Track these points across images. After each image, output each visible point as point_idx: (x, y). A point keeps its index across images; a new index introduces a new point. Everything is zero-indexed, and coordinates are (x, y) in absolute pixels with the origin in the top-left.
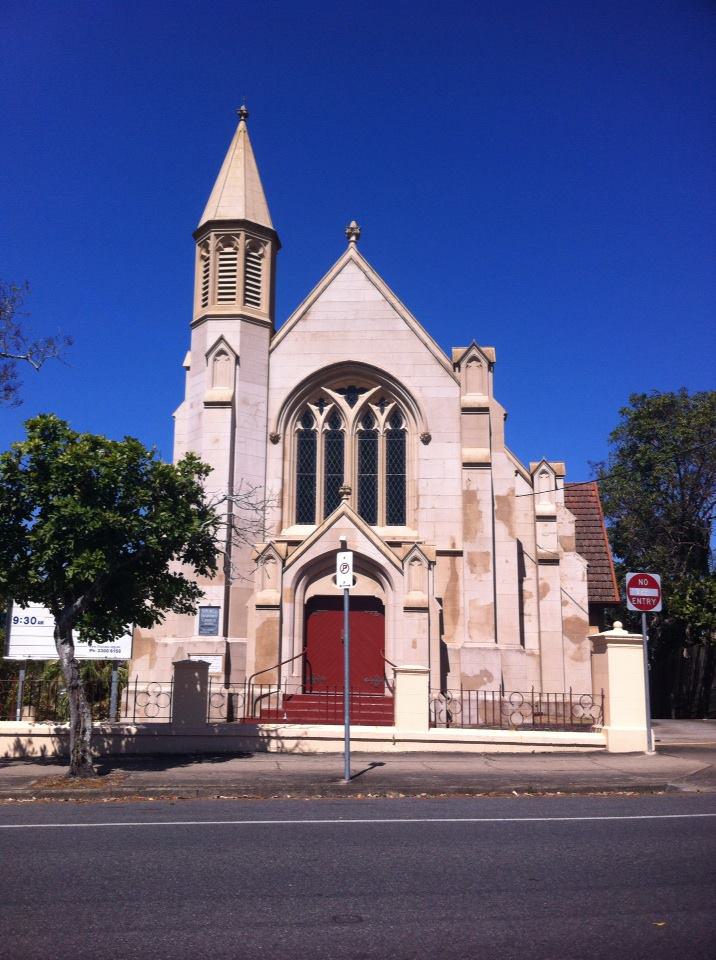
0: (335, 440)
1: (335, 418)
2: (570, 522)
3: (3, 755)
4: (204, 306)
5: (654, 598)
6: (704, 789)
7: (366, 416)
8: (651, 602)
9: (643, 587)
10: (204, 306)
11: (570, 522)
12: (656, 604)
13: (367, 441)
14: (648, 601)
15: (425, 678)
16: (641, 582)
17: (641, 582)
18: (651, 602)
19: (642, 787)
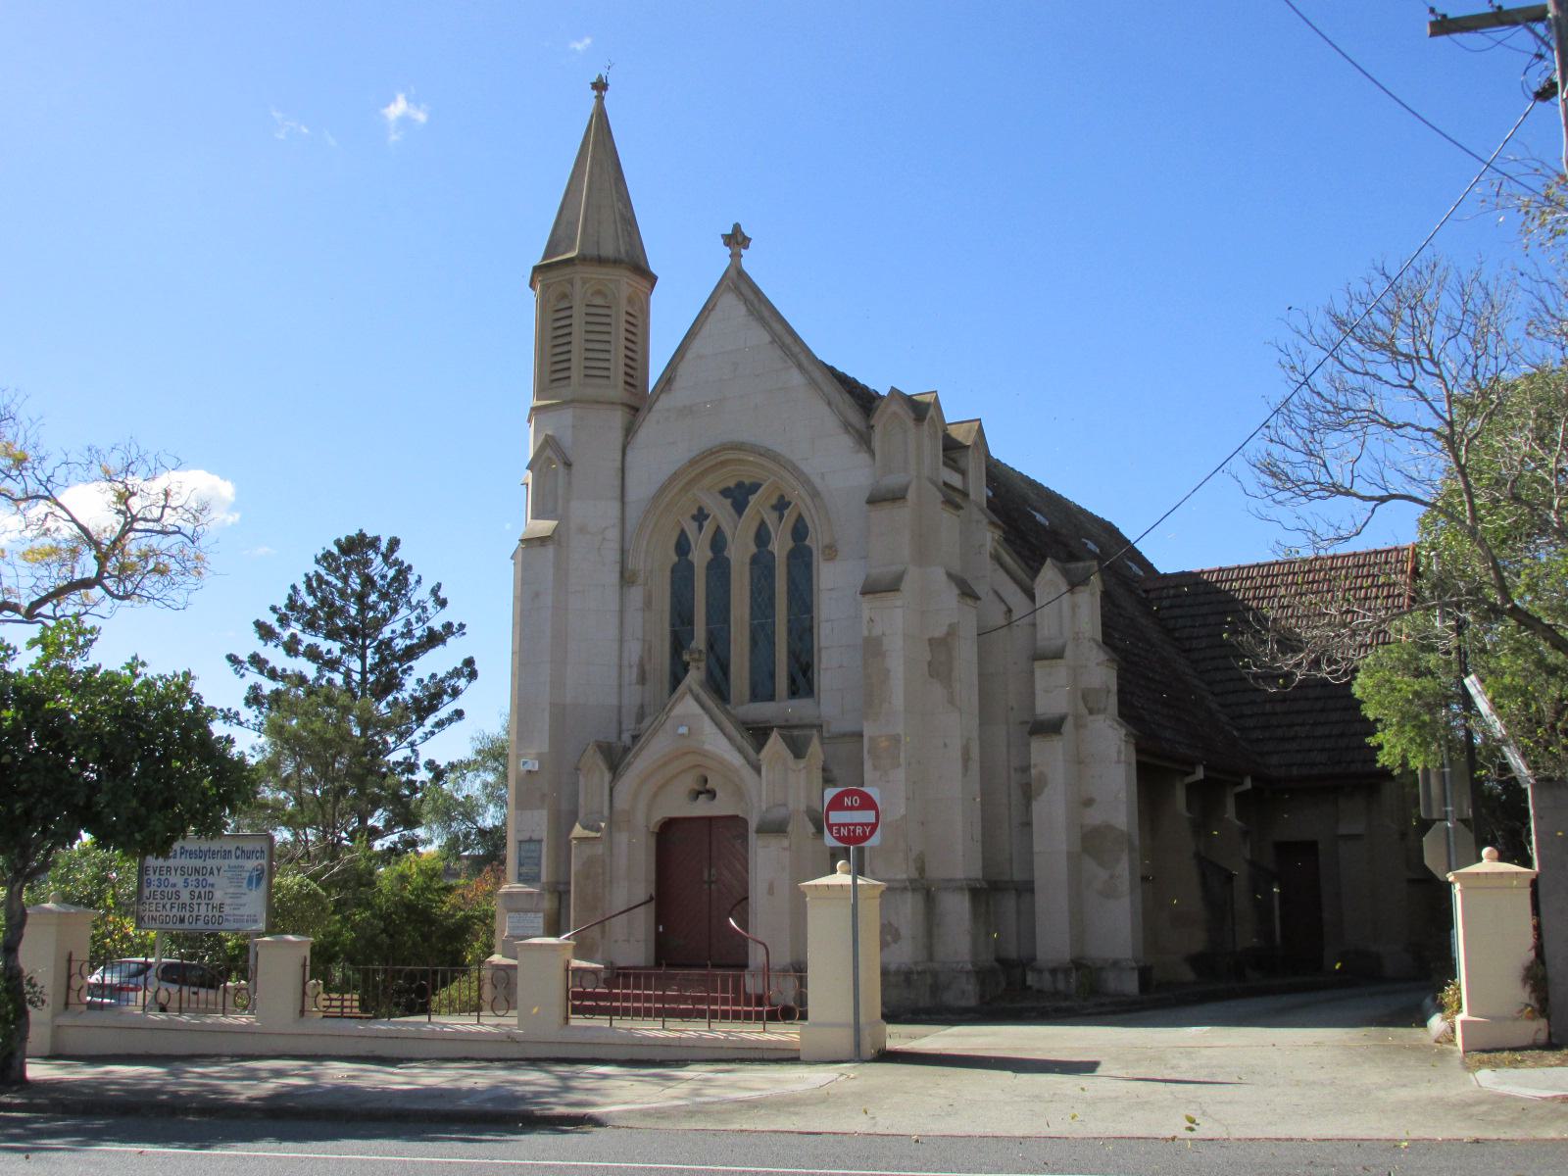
0: (719, 567)
1: (718, 543)
2: (1098, 664)
3: (1062, 730)
4: (233, 659)
5: (867, 825)
6: (787, 1075)
7: (762, 537)
8: (864, 832)
9: (851, 808)
10: (233, 659)
11: (1098, 664)
12: (872, 832)
13: (762, 564)
14: (859, 830)
15: (831, 822)
16: (847, 801)
17: (847, 801)
18: (864, 832)
19: (677, 1017)
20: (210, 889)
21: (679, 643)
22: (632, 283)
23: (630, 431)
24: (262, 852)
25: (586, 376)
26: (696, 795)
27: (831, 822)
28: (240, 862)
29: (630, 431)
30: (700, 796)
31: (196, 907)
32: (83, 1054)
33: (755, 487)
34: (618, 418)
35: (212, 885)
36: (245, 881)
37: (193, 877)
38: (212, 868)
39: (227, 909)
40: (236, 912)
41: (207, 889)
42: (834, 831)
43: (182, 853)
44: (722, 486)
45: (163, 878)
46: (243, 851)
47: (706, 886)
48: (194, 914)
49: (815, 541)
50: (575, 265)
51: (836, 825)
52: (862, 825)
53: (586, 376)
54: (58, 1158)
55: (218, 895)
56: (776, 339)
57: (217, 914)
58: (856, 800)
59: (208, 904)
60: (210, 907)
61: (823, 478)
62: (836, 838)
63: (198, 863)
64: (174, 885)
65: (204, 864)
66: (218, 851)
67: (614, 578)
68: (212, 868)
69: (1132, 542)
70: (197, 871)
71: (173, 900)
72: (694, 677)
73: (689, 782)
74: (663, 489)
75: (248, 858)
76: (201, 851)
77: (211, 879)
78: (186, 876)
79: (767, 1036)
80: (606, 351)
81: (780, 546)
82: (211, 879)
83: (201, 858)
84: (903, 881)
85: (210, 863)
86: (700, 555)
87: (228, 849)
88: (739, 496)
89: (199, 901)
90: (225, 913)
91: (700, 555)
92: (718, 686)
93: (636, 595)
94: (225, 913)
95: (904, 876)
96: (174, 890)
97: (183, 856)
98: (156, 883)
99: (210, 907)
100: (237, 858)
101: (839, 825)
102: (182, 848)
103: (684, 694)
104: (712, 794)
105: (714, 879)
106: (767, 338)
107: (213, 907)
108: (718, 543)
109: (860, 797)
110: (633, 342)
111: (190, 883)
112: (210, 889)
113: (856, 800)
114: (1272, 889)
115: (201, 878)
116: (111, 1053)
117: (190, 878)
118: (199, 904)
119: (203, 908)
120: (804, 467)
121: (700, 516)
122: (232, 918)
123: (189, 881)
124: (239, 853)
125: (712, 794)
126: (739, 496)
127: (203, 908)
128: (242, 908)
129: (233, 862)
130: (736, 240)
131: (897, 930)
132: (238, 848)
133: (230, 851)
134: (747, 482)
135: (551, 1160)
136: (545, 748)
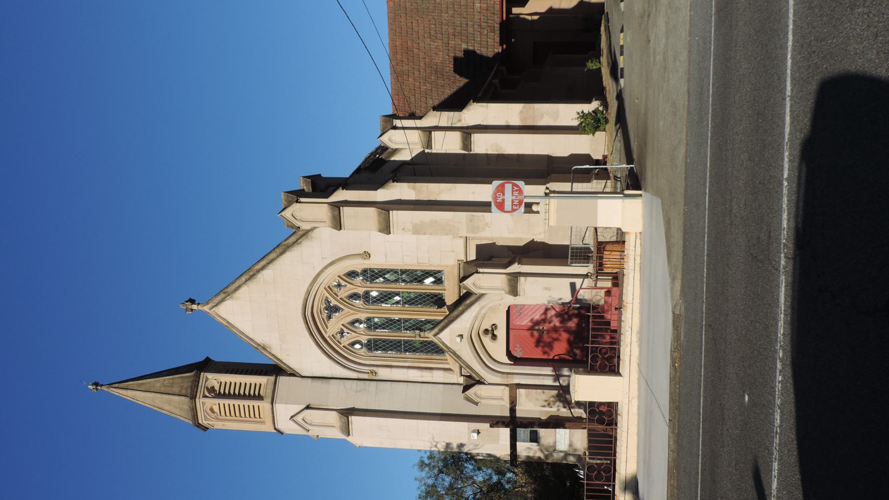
5: (513, 188)
8: (516, 191)
12: (517, 186)
15: (510, 210)
18: (516, 191)
21: (410, 347)
22: (210, 369)
23: (293, 374)
26: (494, 337)
27: (510, 210)
29: (293, 374)
30: (495, 333)
33: (327, 301)
34: (282, 379)
42: (516, 208)
49: (358, 265)
51: (512, 207)
52: (513, 191)
58: (499, 195)
62: (519, 207)
72: (429, 336)
73: (487, 340)
80: (304, 421)
81: (359, 286)
92: (439, 325)
93: (383, 373)
101: (513, 205)
103: (440, 340)
104: (494, 326)
109: (499, 192)
113: (499, 195)
114: (570, 485)
125: (494, 326)
135: (699, 443)
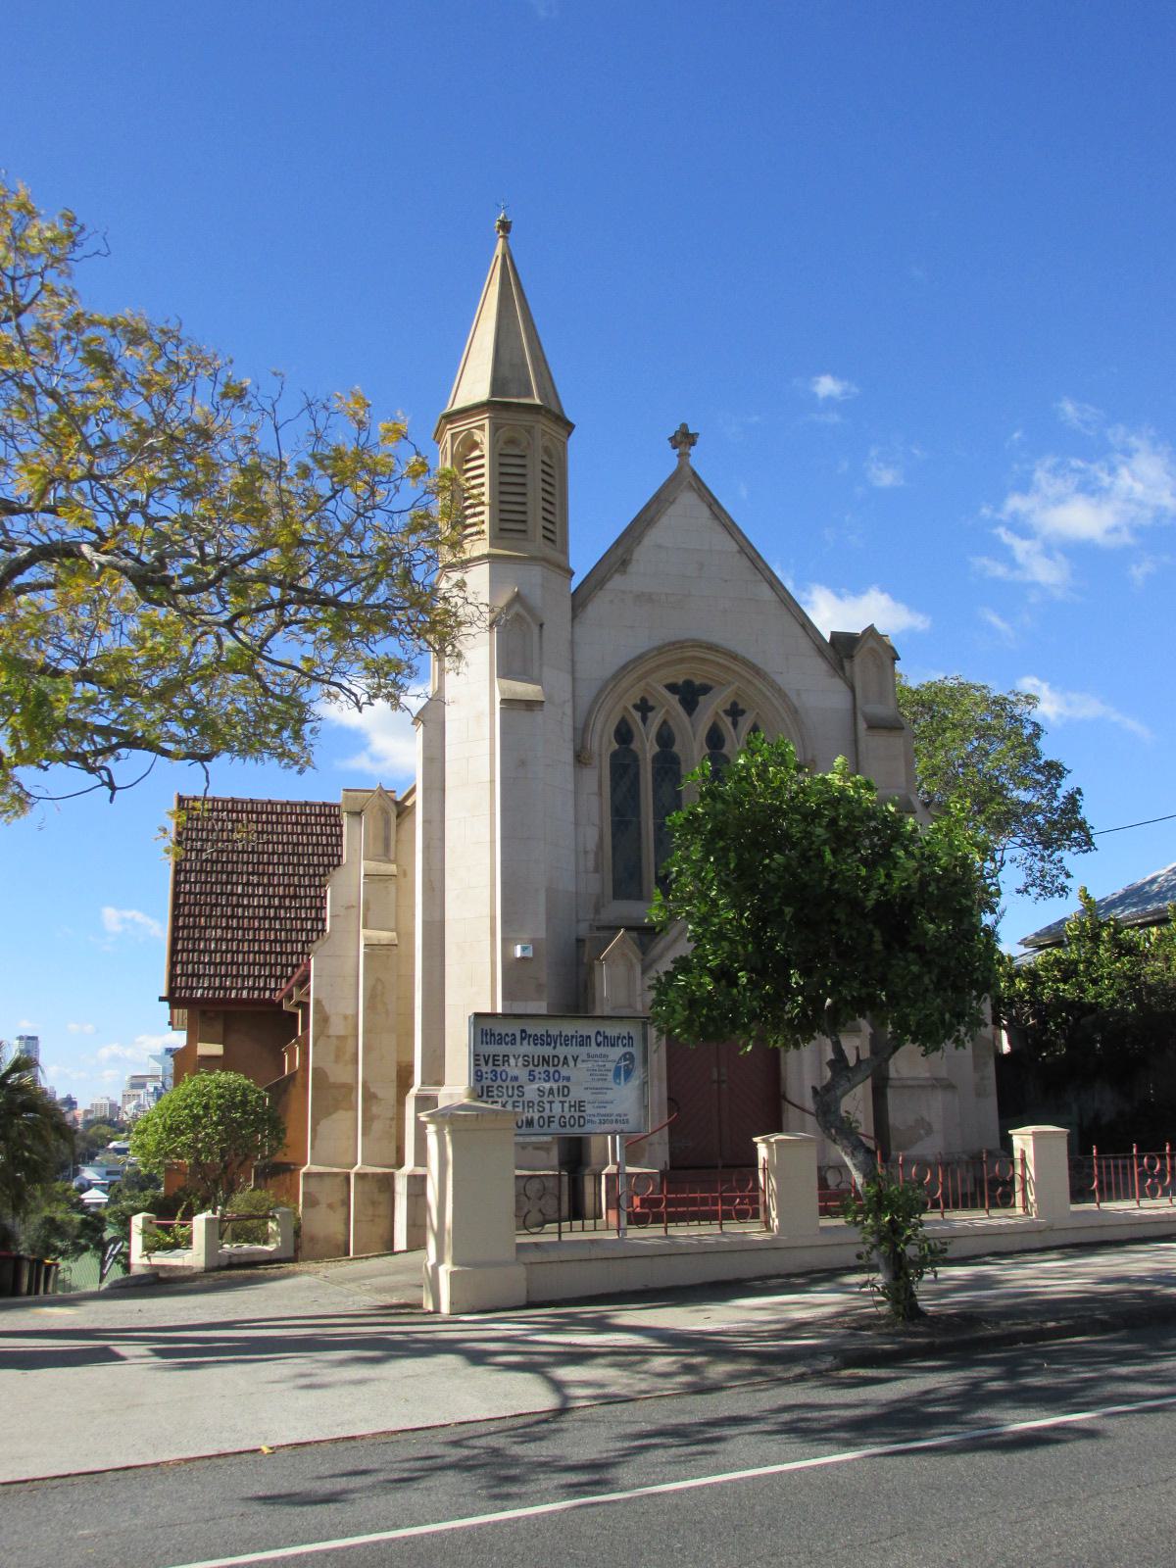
1: (665, 738)
20: (565, 1083)
24: (630, 1038)
25: (501, 530)
28: (602, 1050)
31: (547, 1106)
32: (576, 1295)
35: (568, 1079)
36: (611, 1075)
37: (541, 1069)
38: (565, 1058)
39: (589, 1109)
40: (602, 1111)
41: (561, 1084)
43: (522, 1039)
44: (670, 680)
45: (499, 1069)
46: (606, 1037)
47: (715, 1086)
48: (546, 1114)
50: (538, 413)
53: (501, 530)
54: (669, 1417)
55: (576, 1093)
56: (742, 550)
57: (577, 1115)
59: (562, 1102)
60: (566, 1105)
61: (799, 695)
63: (547, 1051)
64: (516, 1079)
65: (555, 1052)
66: (572, 1037)
67: (568, 756)
68: (565, 1058)
69: (159, 756)
70: (545, 1060)
71: (515, 1098)
74: (624, 669)
75: (613, 1045)
76: (548, 1036)
77: (564, 1071)
78: (531, 1067)
79: (994, 1222)
82: (564, 1071)
83: (549, 1044)
84: (927, 1079)
85: (562, 1051)
86: (647, 747)
87: (585, 1034)
88: (690, 695)
89: (551, 1098)
90: (588, 1112)
91: (647, 747)
94: (588, 1112)
95: (928, 1075)
96: (516, 1084)
97: (525, 1042)
98: (490, 1076)
99: (566, 1105)
100: (598, 1045)
102: (523, 1031)
105: (723, 1078)
106: (735, 548)
107: (570, 1106)
108: (665, 738)
110: (550, 513)
111: (537, 1076)
112: (565, 1083)
115: (552, 1070)
116: (699, 1282)
117: (537, 1070)
118: (551, 1102)
119: (557, 1107)
120: (779, 680)
121: (644, 708)
122: (596, 1119)
123: (536, 1073)
124: (600, 1039)
126: (690, 695)
127: (557, 1107)
128: (609, 1106)
129: (594, 1049)
130: (684, 439)
131: (929, 1124)
132: (598, 1033)
133: (589, 1037)
134: (697, 682)
136: (542, 934)
